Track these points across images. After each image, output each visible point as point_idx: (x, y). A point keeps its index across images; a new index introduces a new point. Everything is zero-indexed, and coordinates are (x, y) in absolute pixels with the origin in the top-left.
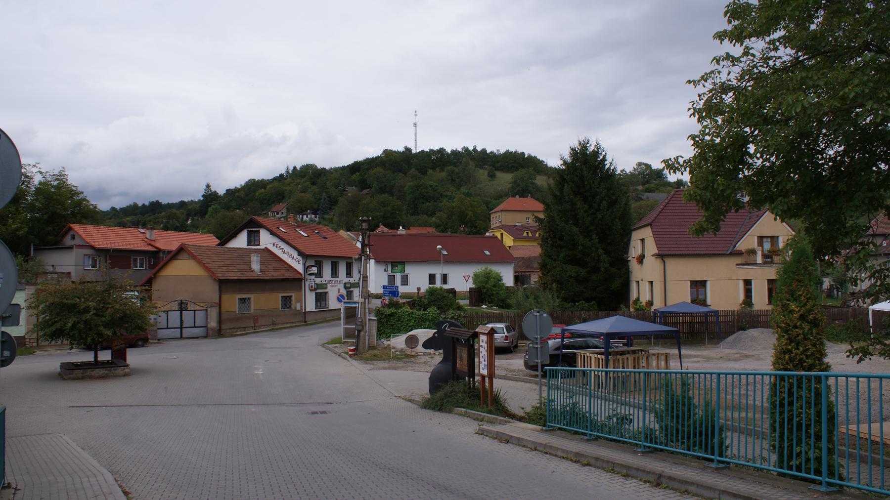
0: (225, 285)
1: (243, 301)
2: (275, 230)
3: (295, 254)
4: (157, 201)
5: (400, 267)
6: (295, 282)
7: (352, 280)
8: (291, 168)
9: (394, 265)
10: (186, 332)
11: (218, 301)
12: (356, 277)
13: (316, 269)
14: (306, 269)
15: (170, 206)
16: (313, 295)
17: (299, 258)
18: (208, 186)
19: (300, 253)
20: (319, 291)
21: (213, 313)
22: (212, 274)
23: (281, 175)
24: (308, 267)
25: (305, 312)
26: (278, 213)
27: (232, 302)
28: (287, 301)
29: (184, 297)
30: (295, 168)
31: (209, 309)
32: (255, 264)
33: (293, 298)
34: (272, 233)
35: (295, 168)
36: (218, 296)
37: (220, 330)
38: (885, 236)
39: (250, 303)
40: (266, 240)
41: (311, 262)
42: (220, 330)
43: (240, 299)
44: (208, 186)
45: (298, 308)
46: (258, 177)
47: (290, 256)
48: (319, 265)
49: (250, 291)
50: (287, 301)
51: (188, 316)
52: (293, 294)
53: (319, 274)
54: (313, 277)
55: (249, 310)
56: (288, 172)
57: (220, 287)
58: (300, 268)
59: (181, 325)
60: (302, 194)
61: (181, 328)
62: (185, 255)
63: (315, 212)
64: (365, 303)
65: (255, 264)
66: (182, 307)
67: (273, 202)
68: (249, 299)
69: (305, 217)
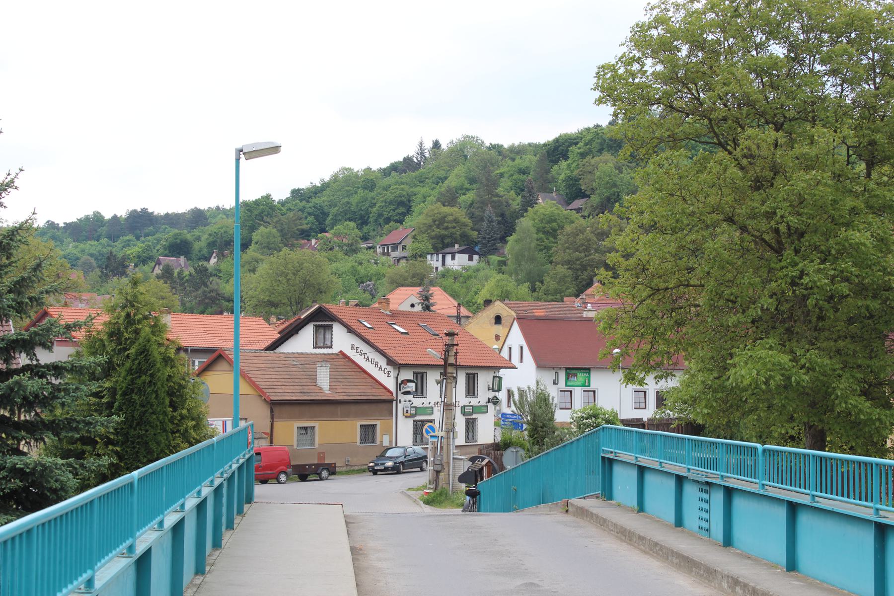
0: (277, 406)
2: (354, 325)
3: (383, 362)
4: (144, 211)
5: (581, 377)
6: (384, 404)
7: (474, 401)
8: (428, 145)
9: (571, 372)
11: (269, 431)
12: (483, 395)
13: (413, 385)
14: (400, 385)
15: (171, 219)
16: (410, 422)
17: (389, 368)
19: (391, 362)
20: (418, 418)
22: (260, 393)
23: (408, 161)
24: (403, 382)
26: (395, 248)
27: (288, 433)
28: (368, 433)
30: (436, 145)
32: (324, 378)
33: (317, 429)
34: (350, 330)
35: (436, 145)
38: (891, 383)
39: (313, 435)
40: (341, 340)
41: (408, 375)
47: (376, 365)
48: (420, 379)
49: (314, 417)
50: (368, 433)
52: (378, 423)
53: (420, 391)
54: (410, 397)
55: (312, 443)
56: (421, 152)
57: (272, 411)
58: (390, 383)
60: (447, 210)
62: (222, 366)
63: (469, 251)
64: (448, 438)
65: (324, 378)
67: (388, 220)
68: (313, 428)
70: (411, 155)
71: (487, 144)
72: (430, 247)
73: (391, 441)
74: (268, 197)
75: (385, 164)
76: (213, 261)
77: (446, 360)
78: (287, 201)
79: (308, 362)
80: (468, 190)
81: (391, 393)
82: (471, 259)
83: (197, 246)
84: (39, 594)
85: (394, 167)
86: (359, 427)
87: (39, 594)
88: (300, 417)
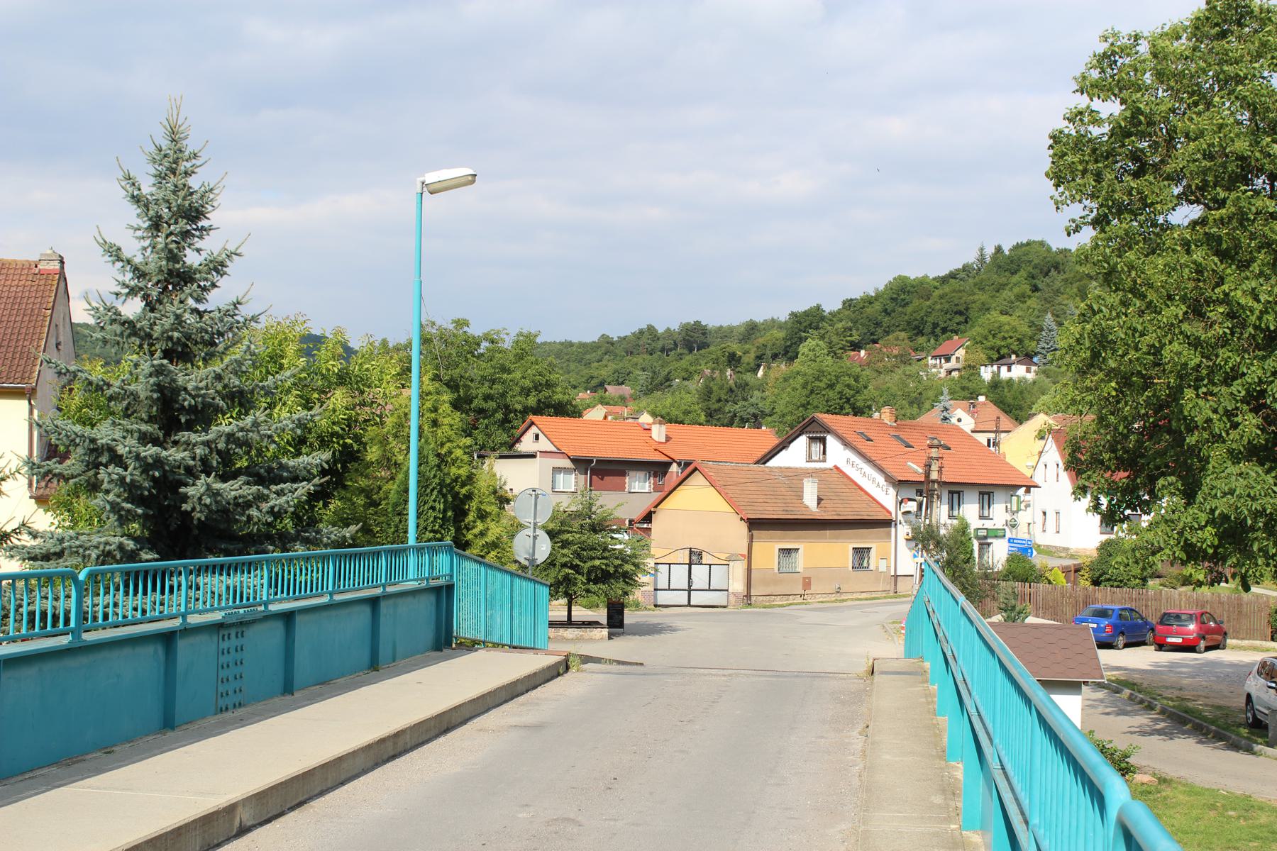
1: (787, 552)
3: (880, 479)
4: (697, 323)
7: (988, 524)
8: (990, 251)
10: (697, 598)
18: (1075, 78)
21: (739, 568)
23: (966, 268)
25: (896, 577)
29: (697, 545)
30: (999, 249)
31: (731, 564)
34: (846, 444)
35: (999, 249)
36: (745, 543)
37: (748, 596)
40: (837, 453)
42: (748, 596)
43: (781, 550)
44: (1075, 78)
45: (883, 568)
46: (914, 273)
50: (861, 553)
51: (699, 572)
52: (873, 546)
59: (690, 586)
61: (689, 590)
66: (695, 557)
69: (1004, 369)
70: (971, 261)
71: (1054, 249)
72: (983, 356)
73: (888, 567)
74: (818, 307)
75: (943, 272)
76: (760, 373)
77: (927, 474)
78: (839, 312)
79: (795, 477)
80: (1030, 297)
81: (890, 513)
82: (1028, 371)
83: (745, 359)
84: (1090, 846)
85: (953, 275)
86: (851, 552)
87: (1090, 846)
88: (781, 539)
